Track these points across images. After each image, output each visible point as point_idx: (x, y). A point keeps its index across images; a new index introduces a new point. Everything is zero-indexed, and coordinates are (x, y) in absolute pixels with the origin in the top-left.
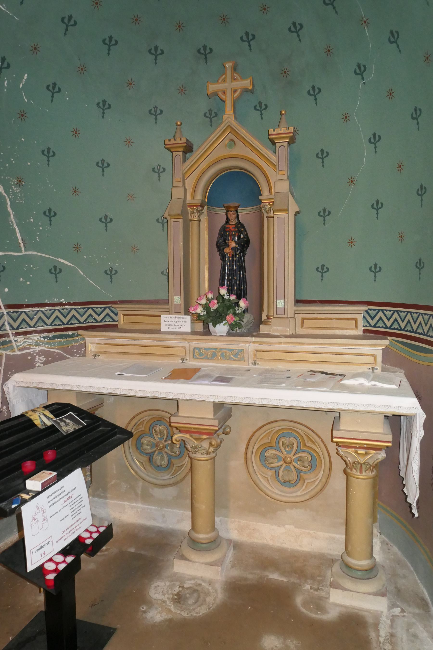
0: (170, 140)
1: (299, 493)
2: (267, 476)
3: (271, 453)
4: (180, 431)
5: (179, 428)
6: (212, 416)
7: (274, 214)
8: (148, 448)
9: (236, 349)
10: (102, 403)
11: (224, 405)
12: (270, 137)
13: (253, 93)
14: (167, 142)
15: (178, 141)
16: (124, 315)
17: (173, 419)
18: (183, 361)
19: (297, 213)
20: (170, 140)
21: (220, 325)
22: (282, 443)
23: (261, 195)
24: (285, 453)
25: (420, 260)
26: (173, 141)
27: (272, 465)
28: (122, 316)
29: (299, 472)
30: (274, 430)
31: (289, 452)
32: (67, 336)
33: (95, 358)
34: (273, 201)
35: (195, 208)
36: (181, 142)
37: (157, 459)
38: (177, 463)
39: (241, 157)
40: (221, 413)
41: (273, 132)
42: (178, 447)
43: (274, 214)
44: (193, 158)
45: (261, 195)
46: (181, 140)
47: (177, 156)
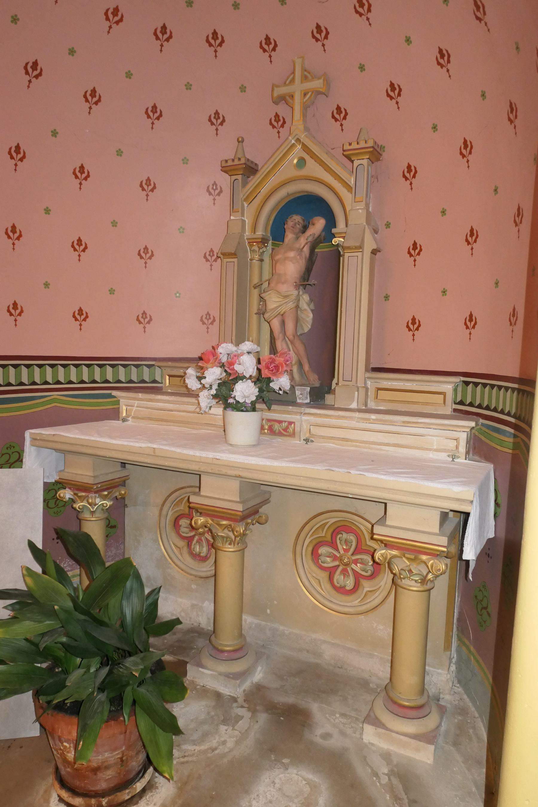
0: (350, 144)
1: (204, 569)
2: (318, 578)
3: (323, 550)
4: (387, 545)
5: (200, 511)
6: (436, 530)
7: (345, 251)
8: (329, 563)
9: (285, 422)
10: (268, 499)
11: (262, 486)
12: (345, 153)
13: (327, 97)
14: (347, 147)
15: (362, 144)
16: (170, 376)
17: (378, 530)
18: (307, 443)
19: (374, 252)
20: (350, 144)
21: (192, 386)
22: (339, 540)
23: (335, 227)
24: (342, 552)
25: (471, 316)
26: (354, 146)
27: (325, 565)
28: (167, 377)
29: (358, 577)
30: (328, 522)
31: (346, 551)
32: (497, 430)
33: (306, 443)
34: (345, 235)
35: (254, 244)
36: (367, 145)
37: (338, 578)
38: (367, 586)
39: (312, 179)
40: (450, 526)
41: (348, 147)
42: (370, 564)
43: (344, 253)
44: (254, 180)
45: (335, 227)
46: (358, 143)
47: (361, 165)
